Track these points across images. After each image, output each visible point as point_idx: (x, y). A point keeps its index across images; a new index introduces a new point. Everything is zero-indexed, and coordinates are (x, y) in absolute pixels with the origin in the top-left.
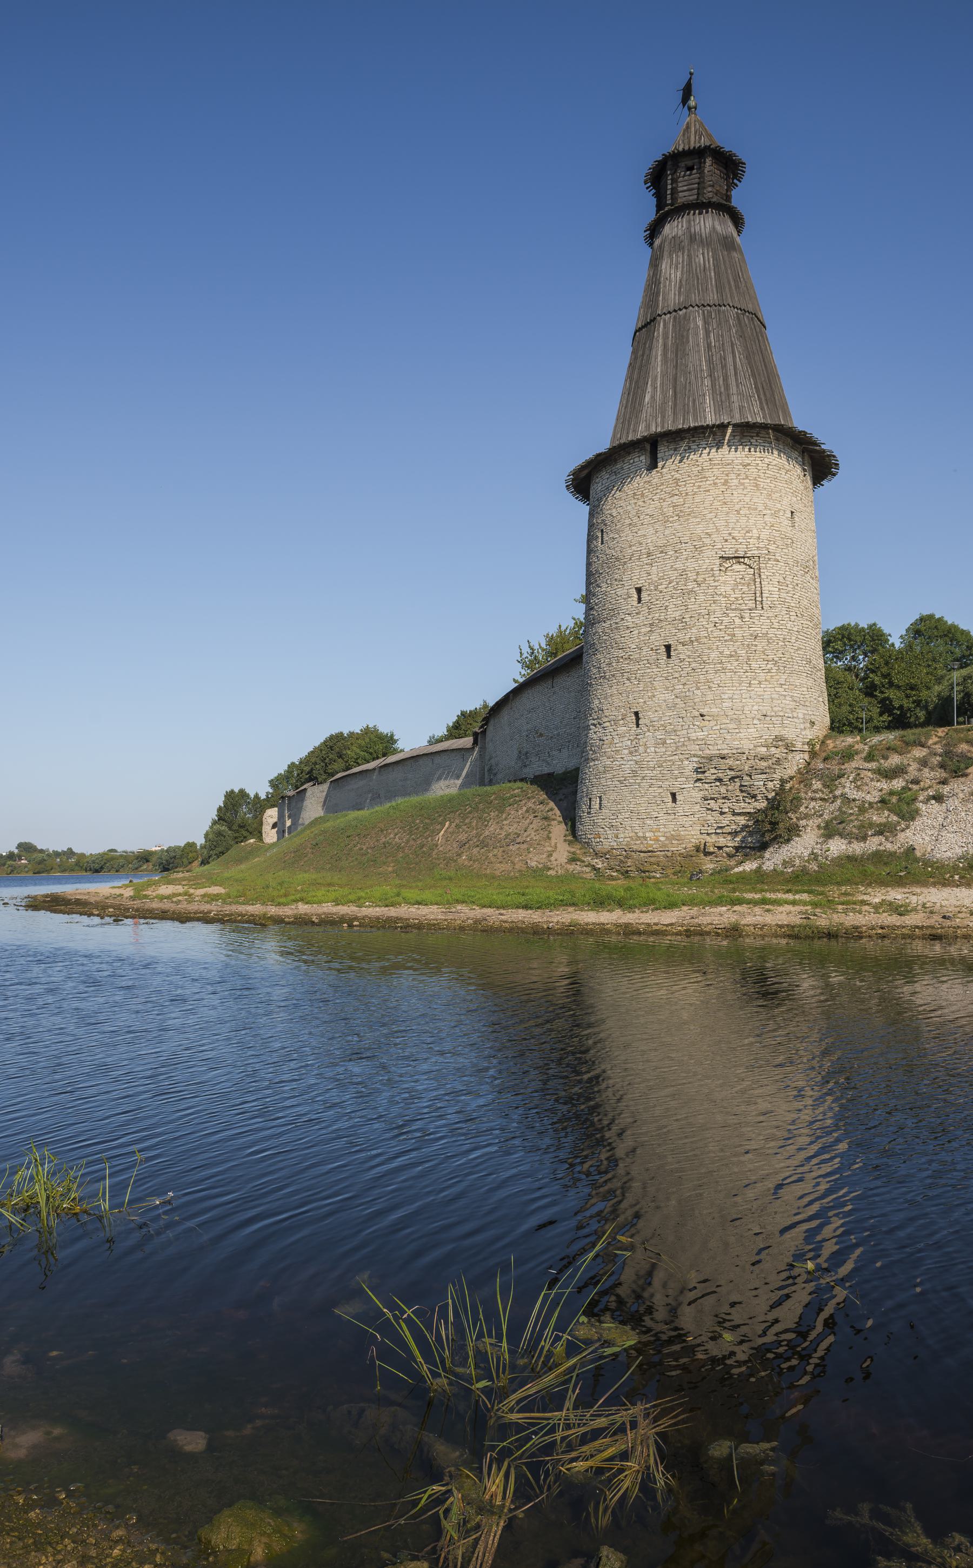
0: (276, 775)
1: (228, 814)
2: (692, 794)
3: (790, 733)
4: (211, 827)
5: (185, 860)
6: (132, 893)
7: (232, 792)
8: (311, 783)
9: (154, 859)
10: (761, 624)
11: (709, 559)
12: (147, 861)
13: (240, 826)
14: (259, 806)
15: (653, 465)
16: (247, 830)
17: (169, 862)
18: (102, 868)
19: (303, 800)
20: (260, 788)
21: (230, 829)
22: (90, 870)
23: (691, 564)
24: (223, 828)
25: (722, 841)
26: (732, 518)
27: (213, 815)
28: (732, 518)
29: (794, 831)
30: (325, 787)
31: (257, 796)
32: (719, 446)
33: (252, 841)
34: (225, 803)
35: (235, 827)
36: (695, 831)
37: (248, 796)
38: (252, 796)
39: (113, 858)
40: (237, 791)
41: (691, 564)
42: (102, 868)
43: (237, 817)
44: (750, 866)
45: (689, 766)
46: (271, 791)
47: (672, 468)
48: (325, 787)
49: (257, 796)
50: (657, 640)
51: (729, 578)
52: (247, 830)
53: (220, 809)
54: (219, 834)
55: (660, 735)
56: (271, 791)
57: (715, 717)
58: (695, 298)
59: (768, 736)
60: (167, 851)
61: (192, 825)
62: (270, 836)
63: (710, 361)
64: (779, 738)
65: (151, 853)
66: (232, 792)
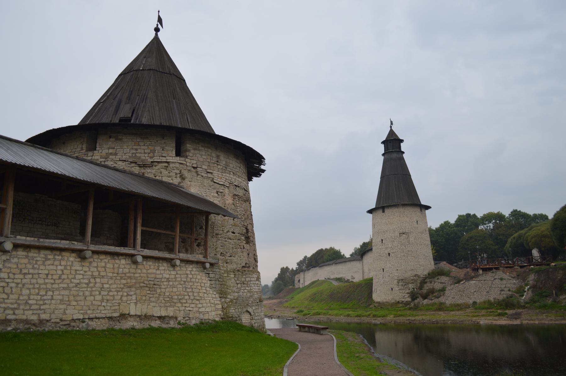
3: (419, 273)
31: (292, 269)
38: (291, 269)
49: (292, 269)
51: (402, 238)
64: (416, 275)
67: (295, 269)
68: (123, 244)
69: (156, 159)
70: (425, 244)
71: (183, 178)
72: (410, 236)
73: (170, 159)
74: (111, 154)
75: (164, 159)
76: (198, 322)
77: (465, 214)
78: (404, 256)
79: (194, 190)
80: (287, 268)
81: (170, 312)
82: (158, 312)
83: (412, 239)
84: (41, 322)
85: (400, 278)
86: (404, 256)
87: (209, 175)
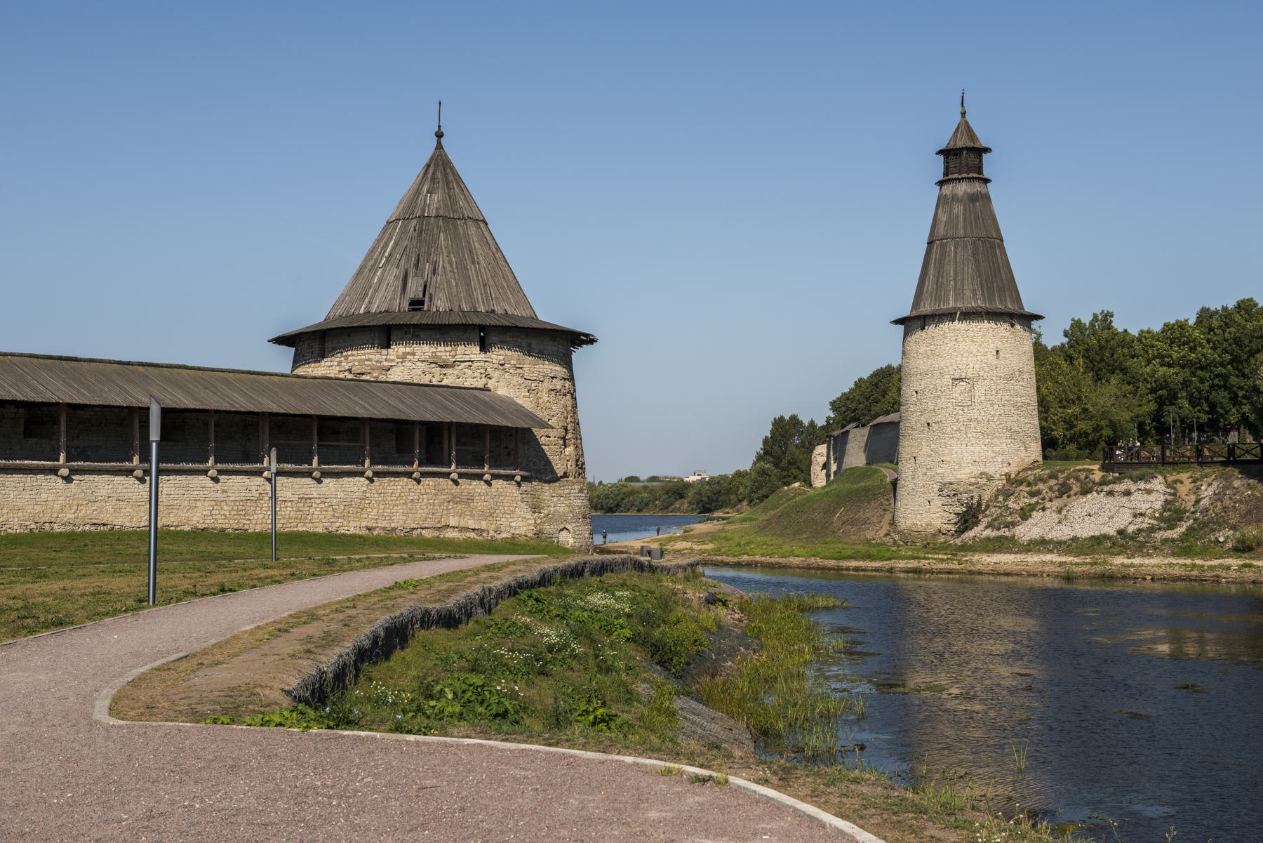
0: (839, 395)
1: (776, 448)
2: (938, 502)
3: (991, 470)
4: (754, 464)
5: (732, 497)
6: (555, 640)
7: (782, 418)
8: (854, 424)
9: (691, 493)
10: (974, 414)
11: (947, 380)
12: (682, 497)
13: (790, 463)
14: (813, 435)
15: (923, 329)
16: (798, 468)
17: (712, 498)
18: (618, 505)
19: (846, 443)
20: (818, 413)
21: (776, 466)
22: (602, 508)
23: (939, 382)
24: (767, 466)
25: (950, 527)
26: (959, 358)
27: (758, 447)
28: (959, 358)
29: (977, 523)
30: (866, 431)
31: (812, 423)
32: (953, 320)
33: (797, 485)
34: (772, 432)
35: (784, 464)
36: (939, 521)
37: (801, 423)
38: (806, 423)
39: (633, 492)
40: (787, 418)
41: (939, 382)
42: (618, 505)
43: (786, 446)
44: (958, 541)
45: (936, 487)
46: (832, 415)
47: (931, 330)
48: (866, 431)
49: (812, 423)
50: (923, 419)
51: (958, 389)
52: (798, 468)
53: (766, 441)
54: (763, 473)
55: (924, 470)
56: (832, 415)
57: (949, 462)
58: (950, 233)
59: (977, 471)
60: (709, 483)
61: (738, 454)
62: (819, 479)
63: (956, 272)
64: (982, 474)
65: (688, 486)
66: (782, 418)
67: (821, 422)
68: (441, 464)
69: (459, 358)
70: (1014, 405)
71: (488, 377)
72: (976, 386)
73: (474, 358)
74: (408, 353)
75: (467, 358)
76: (509, 536)
77: (1157, 328)
78: (959, 430)
79: (502, 392)
80: (794, 418)
81: (484, 525)
82: (471, 524)
83: (979, 394)
84: (394, 529)
85: (947, 480)
86: (959, 430)
87: (519, 371)
